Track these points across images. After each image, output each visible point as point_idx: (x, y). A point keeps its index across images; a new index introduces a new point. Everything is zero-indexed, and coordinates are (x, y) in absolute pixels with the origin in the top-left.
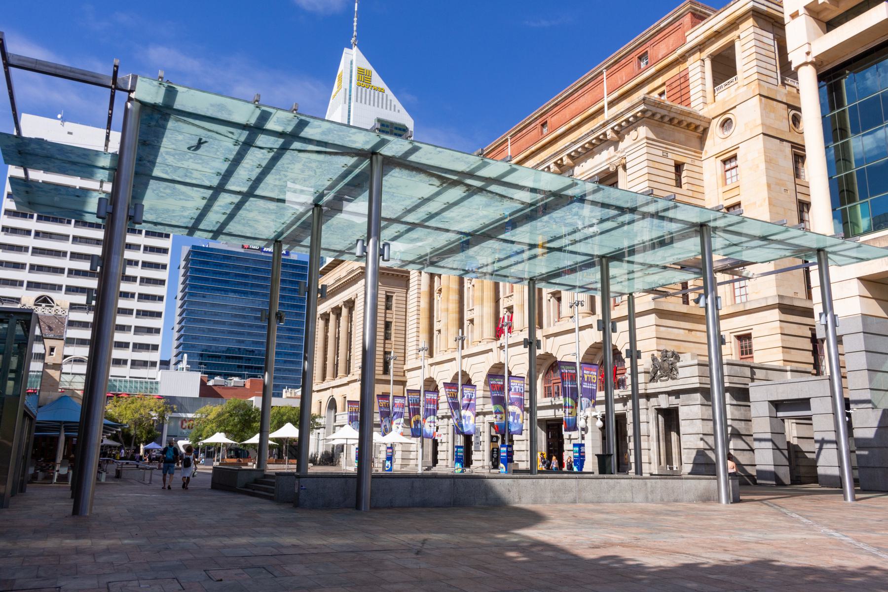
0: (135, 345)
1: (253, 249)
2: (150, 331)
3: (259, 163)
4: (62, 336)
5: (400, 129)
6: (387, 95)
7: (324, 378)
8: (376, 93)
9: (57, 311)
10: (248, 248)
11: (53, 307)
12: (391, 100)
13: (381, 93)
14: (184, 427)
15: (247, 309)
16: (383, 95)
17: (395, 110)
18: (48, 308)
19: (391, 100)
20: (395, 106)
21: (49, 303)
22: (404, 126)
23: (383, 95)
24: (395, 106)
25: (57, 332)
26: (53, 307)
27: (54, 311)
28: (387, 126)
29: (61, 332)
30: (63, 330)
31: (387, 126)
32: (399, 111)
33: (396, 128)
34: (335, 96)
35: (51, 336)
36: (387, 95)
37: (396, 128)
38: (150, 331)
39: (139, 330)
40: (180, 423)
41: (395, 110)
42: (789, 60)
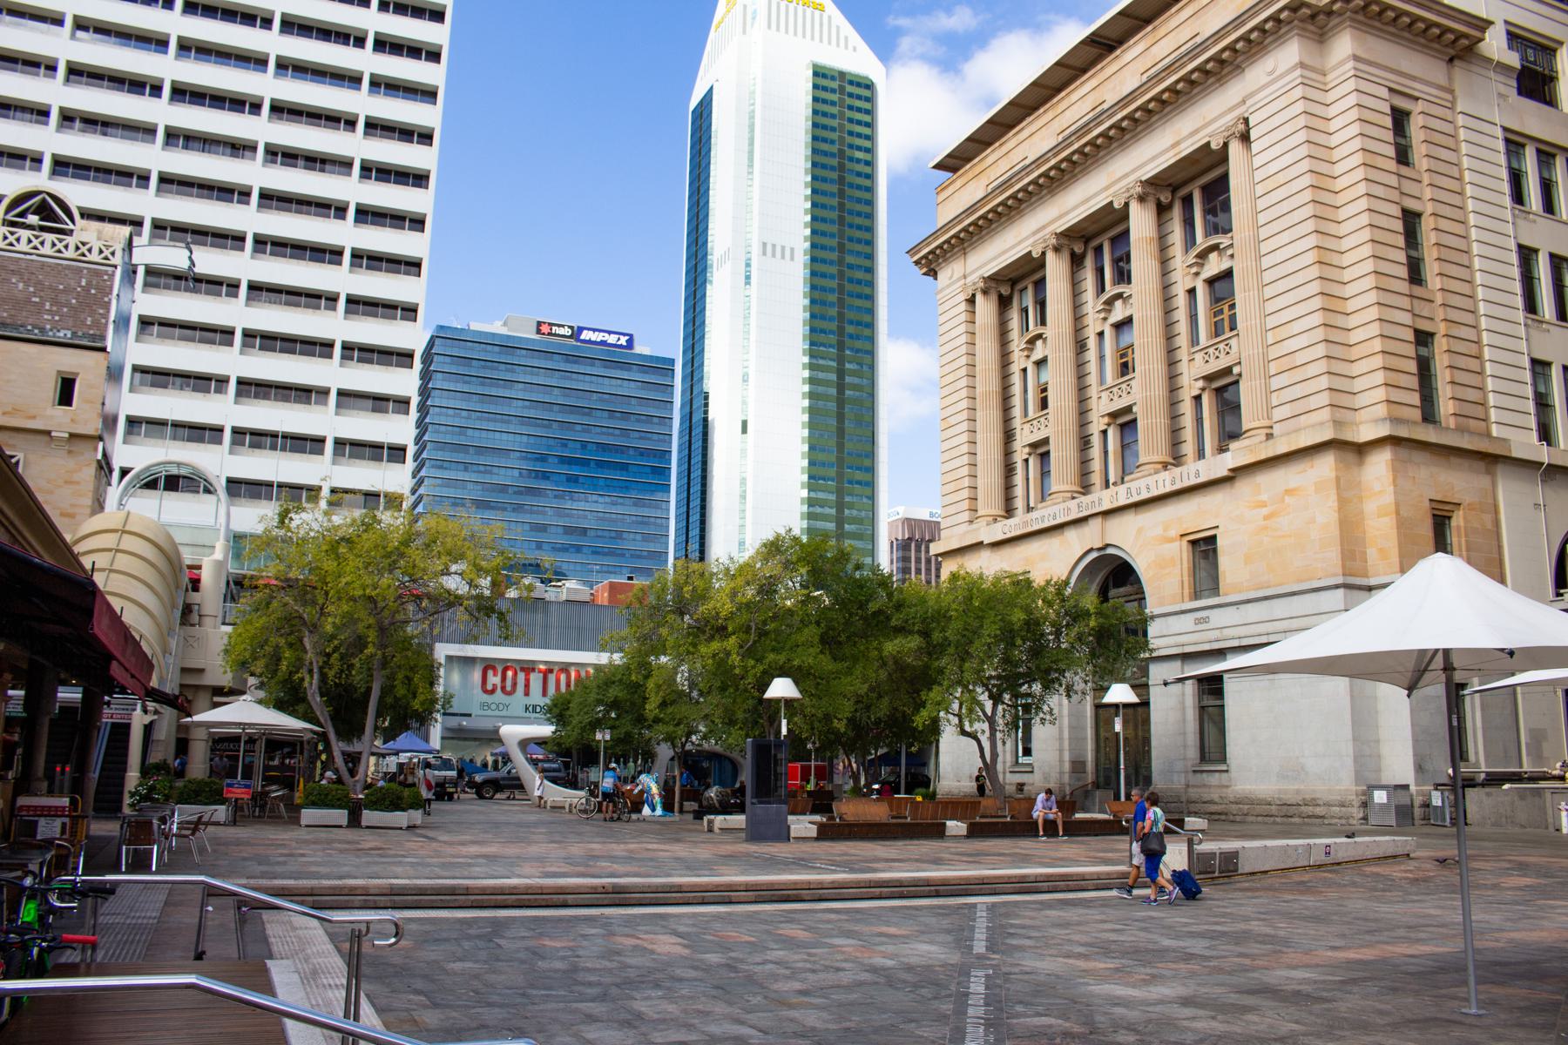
0: (357, 255)
1: (559, 335)
2: (379, 402)
3: (209, 954)
4: (103, 338)
5: (859, 85)
6: (830, 17)
7: (1201, 454)
8: (809, 11)
9: (84, 249)
10: (549, 334)
11: (70, 232)
12: (838, 28)
13: (817, 13)
14: (489, 687)
15: (550, 460)
16: (821, 16)
17: (846, 47)
18: (50, 237)
19: (838, 28)
20: (846, 38)
21: (57, 219)
22: (867, 78)
23: (821, 16)
24: (846, 38)
25: (83, 323)
26: (70, 232)
27: (72, 247)
28: (833, 78)
29: (96, 324)
30: (106, 316)
31: (833, 78)
32: (855, 49)
33: (851, 83)
34: (720, 23)
35: (63, 335)
36: (830, 17)
37: (851, 83)
38: (379, 402)
39: (368, 215)
40: (477, 675)
41: (846, 47)
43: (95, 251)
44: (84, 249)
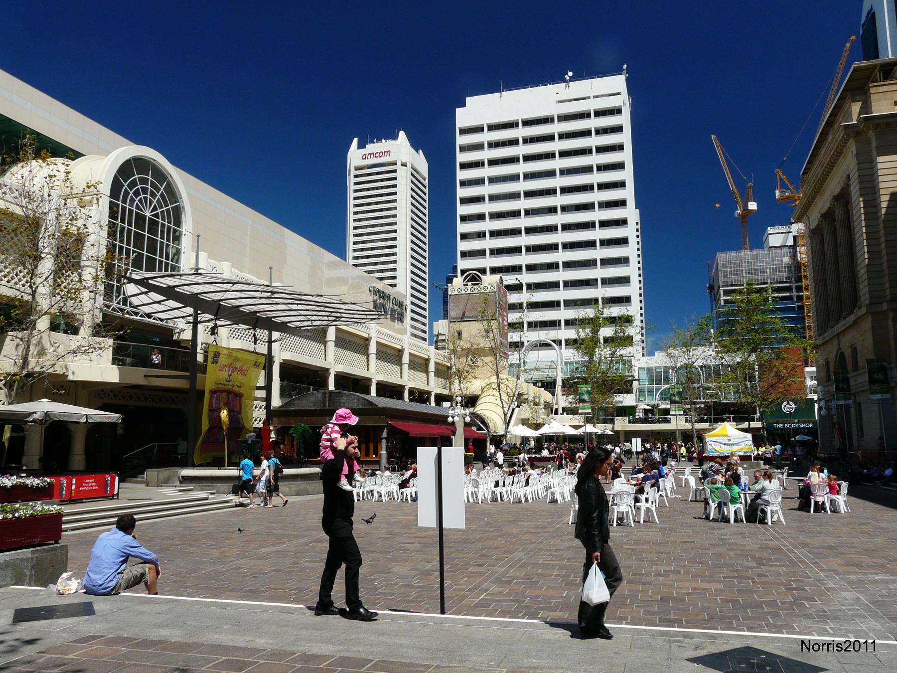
18: (476, 287)
42: (469, 100)
43: (463, 290)
44: (486, 288)
